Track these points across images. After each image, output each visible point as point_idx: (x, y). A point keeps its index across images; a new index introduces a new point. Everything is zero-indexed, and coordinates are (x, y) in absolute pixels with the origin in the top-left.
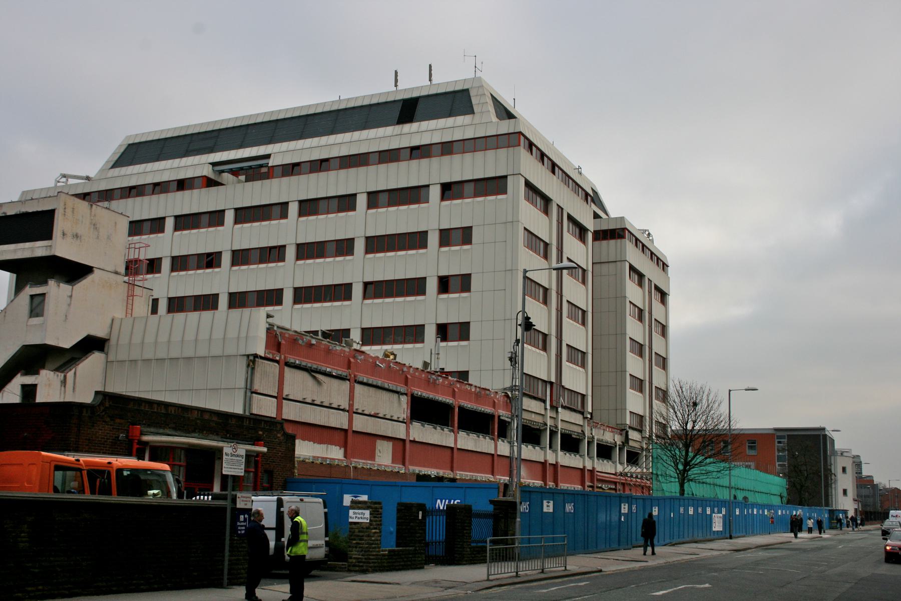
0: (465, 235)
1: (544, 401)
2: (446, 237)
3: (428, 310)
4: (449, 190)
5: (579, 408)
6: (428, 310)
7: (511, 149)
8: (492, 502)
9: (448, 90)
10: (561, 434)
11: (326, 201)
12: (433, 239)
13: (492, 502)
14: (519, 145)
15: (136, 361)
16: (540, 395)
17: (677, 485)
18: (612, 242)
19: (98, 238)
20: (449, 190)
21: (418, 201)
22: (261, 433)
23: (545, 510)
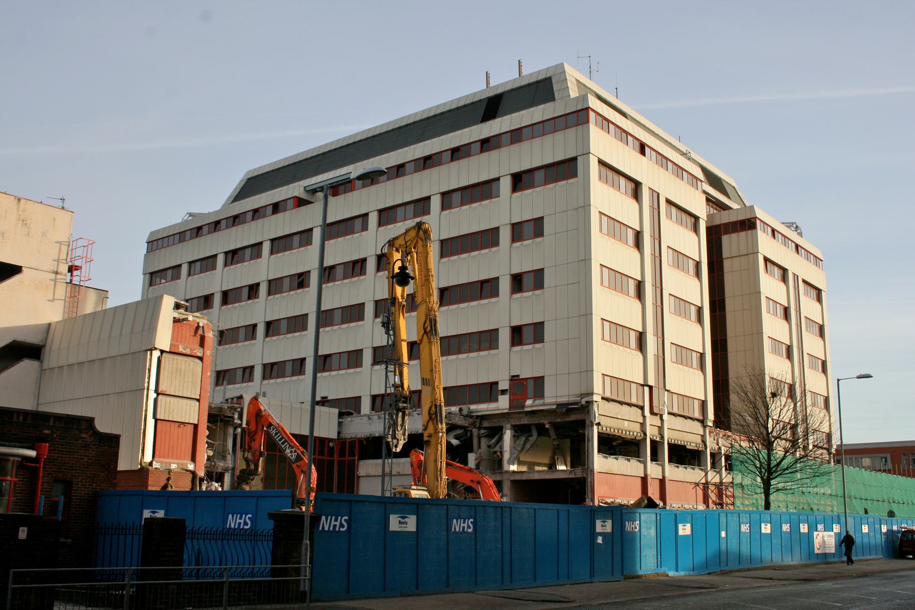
0: (537, 227)
1: (642, 408)
2: (518, 231)
3: (502, 312)
4: (520, 181)
5: (697, 415)
6: (502, 312)
7: (580, 127)
8: (271, 516)
9: (531, 81)
10: (669, 444)
11: (402, 208)
12: (505, 235)
13: (271, 516)
14: (588, 122)
15: (62, 367)
16: (634, 401)
17: (763, 496)
18: (743, 234)
19: (28, 234)
20: (520, 181)
21: (489, 196)
22: (46, 432)
23: (763, 531)
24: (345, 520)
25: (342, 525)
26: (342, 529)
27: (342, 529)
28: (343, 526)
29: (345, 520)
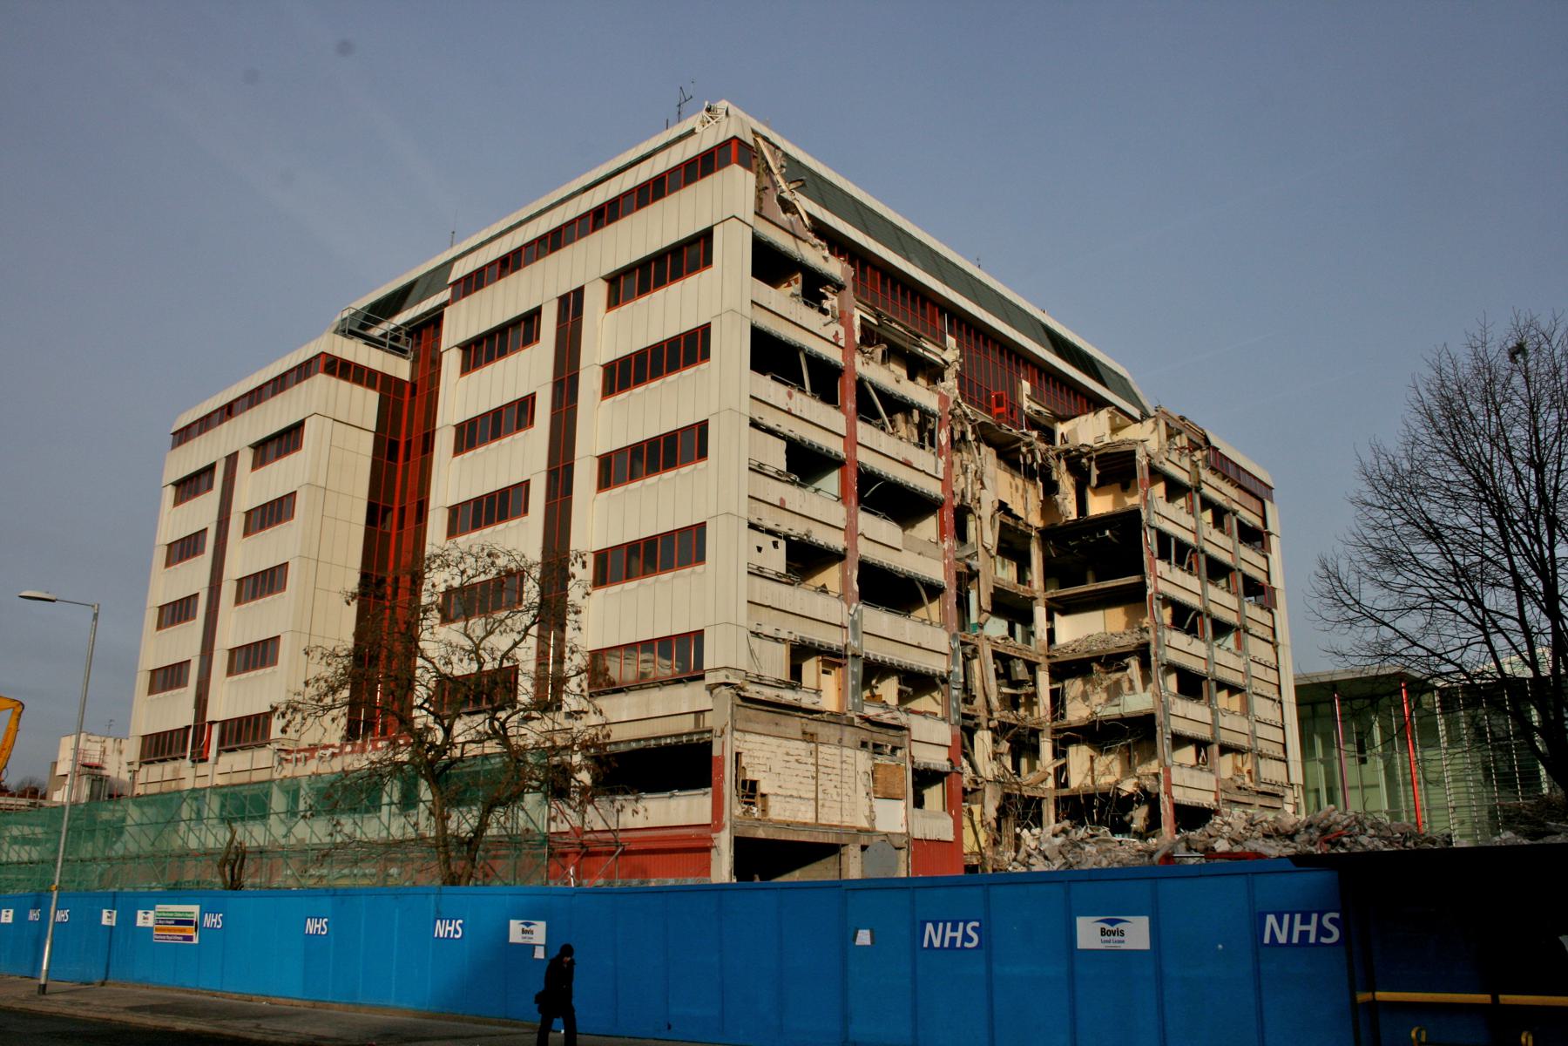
24: (974, 928)
25: (967, 938)
26: (1323, 940)
27: (1323, 940)
28: (1329, 934)
29: (974, 928)
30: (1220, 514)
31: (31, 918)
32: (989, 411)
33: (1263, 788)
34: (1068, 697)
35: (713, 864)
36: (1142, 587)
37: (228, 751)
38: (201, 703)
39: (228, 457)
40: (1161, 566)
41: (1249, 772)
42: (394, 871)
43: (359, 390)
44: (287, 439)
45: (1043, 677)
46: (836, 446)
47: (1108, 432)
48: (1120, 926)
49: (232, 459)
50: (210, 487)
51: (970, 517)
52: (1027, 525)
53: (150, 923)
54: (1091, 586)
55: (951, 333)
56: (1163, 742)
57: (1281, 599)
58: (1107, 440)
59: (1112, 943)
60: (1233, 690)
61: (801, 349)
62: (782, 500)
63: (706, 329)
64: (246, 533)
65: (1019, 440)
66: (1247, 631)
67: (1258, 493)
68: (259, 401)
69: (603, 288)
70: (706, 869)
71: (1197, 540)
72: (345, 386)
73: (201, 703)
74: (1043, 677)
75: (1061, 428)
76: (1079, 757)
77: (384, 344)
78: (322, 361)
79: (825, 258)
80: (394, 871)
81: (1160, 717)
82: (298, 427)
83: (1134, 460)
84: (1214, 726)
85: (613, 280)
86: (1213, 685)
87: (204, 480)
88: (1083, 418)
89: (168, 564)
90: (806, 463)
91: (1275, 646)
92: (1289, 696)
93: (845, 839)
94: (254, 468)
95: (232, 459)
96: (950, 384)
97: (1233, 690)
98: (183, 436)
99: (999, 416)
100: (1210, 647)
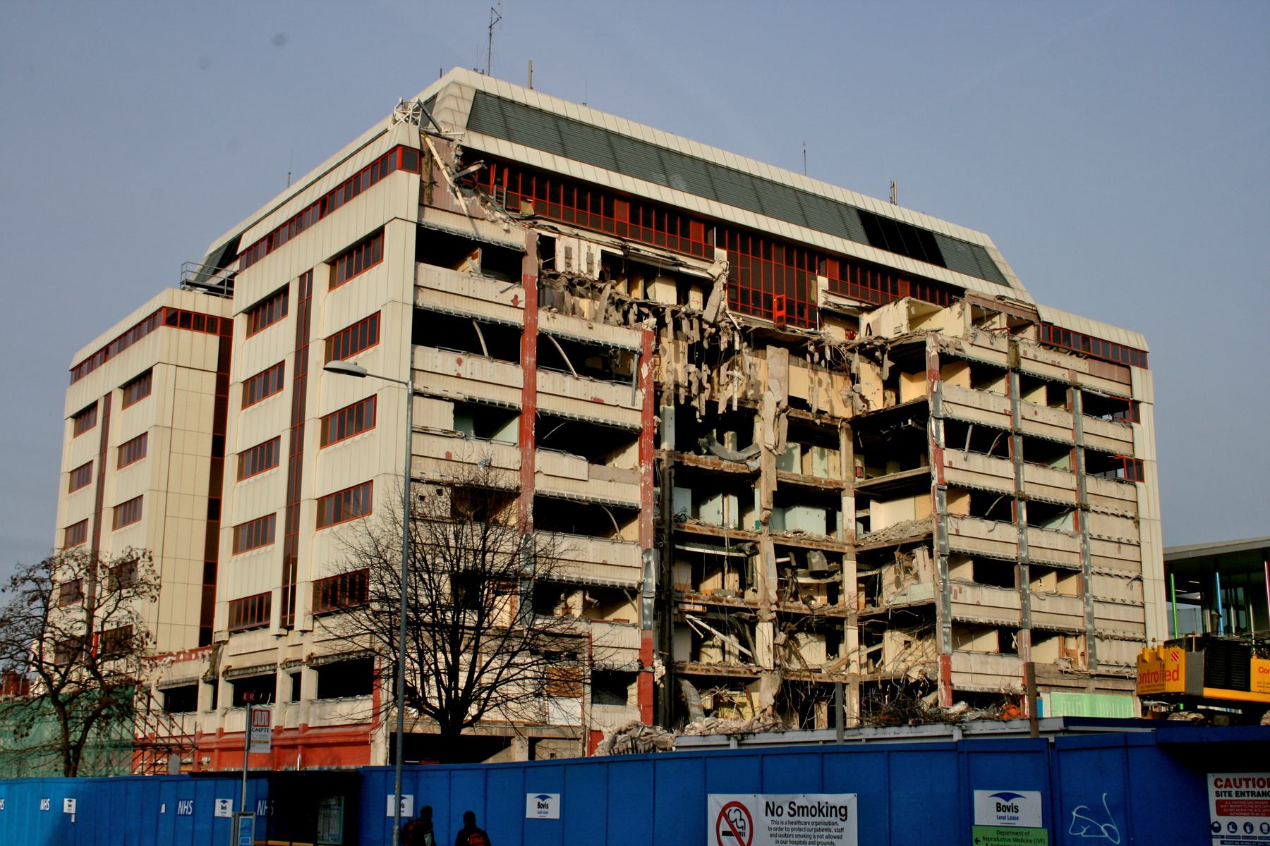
30: (1057, 393)
31: (42, 807)
32: (769, 316)
33: (1102, 670)
34: (885, 583)
35: (372, 754)
36: (927, 477)
37: (237, 632)
38: (290, 561)
39: (302, 277)
40: (950, 455)
41: (1083, 654)
42: (205, 759)
43: (199, 336)
44: (139, 385)
45: (850, 566)
46: (514, 399)
47: (905, 322)
48: (1015, 801)
49: (306, 279)
50: (285, 313)
51: (756, 418)
52: (833, 417)
53: (229, 813)
54: (892, 476)
55: (720, 245)
56: (943, 629)
57: (1149, 471)
58: (905, 330)
59: (1006, 820)
60: (1063, 573)
61: (474, 318)
62: (448, 454)
63: (375, 317)
64: (120, 466)
65: (806, 339)
66: (1086, 509)
67: (1127, 359)
68: (357, 192)
69: (326, 269)
70: (368, 756)
71: (1014, 422)
72: (185, 333)
73: (290, 561)
74: (850, 566)
75: (865, 319)
76: (892, 642)
77: (221, 291)
78: (161, 317)
79: (507, 231)
80: (205, 759)
81: (940, 609)
82: (148, 373)
83: (924, 351)
84: (1025, 610)
85: (333, 262)
86: (1026, 569)
87: (278, 305)
88: (885, 308)
89: (71, 490)
90: (481, 418)
91: (1136, 521)
92: (1155, 571)
93: (510, 732)
94: (249, 335)
95: (306, 279)
96: (719, 296)
97: (1063, 573)
98: (79, 372)
99: (780, 319)
100: (1021, 531)
